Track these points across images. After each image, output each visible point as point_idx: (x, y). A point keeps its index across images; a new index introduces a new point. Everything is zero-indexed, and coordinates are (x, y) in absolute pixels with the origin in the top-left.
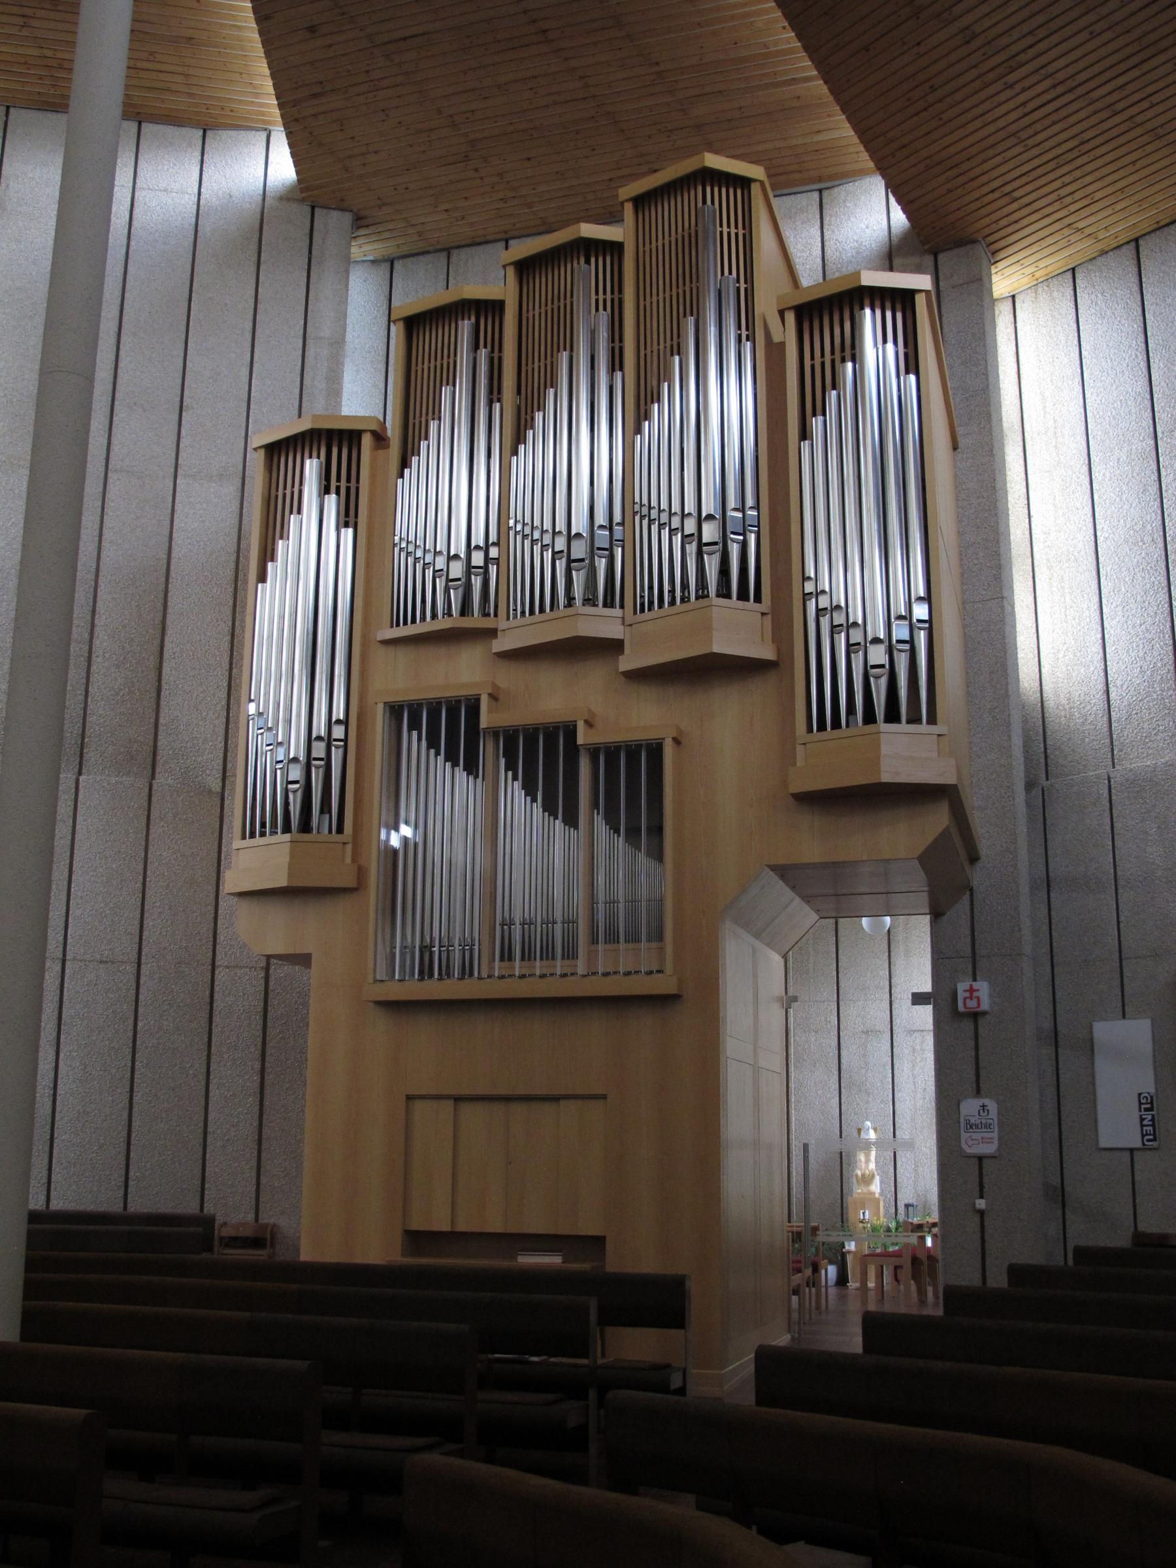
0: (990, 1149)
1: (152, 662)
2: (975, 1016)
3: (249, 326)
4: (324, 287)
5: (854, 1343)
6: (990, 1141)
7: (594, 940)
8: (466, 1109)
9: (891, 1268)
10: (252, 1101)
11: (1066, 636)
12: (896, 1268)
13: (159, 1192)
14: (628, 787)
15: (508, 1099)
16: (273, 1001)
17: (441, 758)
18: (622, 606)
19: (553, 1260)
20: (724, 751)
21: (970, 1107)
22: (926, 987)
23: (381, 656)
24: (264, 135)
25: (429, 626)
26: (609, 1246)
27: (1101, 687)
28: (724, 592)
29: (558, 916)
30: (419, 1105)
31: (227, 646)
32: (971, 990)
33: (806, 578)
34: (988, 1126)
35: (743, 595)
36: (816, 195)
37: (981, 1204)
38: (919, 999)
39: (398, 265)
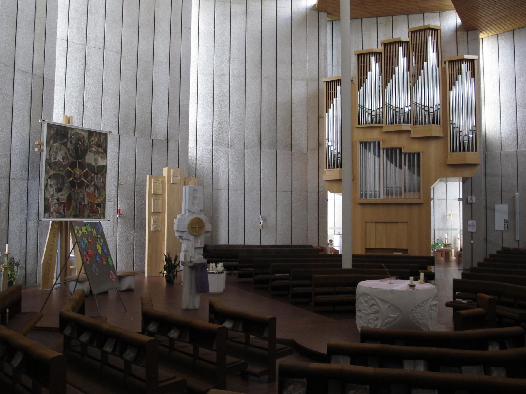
0: (474, 231)
1: (290, 124)
2: (472, 204)
4: (322, 32)
5: (411, 277)
6: (473, 229)
7: (405, 191)
9: (440, 255)
10: (316, 221)
12: (442, 254)
13: (298, 241)
14: (414, 161)
15: (386, 222)
16: (320, 200)
20: (432, 153)
21: (470, 222)
22: (461, 197)
23: (356, 131)
25: (367, 125)
26: (409, 251)
27: (500, 133)
28: (433, 123)
30: (368, 224)
31: (306, 120)
32: (471, 198)
33: (450, 121)
35: (437, 123)
36: (438, 13)
38: (459, 199)
39: (334, 22)
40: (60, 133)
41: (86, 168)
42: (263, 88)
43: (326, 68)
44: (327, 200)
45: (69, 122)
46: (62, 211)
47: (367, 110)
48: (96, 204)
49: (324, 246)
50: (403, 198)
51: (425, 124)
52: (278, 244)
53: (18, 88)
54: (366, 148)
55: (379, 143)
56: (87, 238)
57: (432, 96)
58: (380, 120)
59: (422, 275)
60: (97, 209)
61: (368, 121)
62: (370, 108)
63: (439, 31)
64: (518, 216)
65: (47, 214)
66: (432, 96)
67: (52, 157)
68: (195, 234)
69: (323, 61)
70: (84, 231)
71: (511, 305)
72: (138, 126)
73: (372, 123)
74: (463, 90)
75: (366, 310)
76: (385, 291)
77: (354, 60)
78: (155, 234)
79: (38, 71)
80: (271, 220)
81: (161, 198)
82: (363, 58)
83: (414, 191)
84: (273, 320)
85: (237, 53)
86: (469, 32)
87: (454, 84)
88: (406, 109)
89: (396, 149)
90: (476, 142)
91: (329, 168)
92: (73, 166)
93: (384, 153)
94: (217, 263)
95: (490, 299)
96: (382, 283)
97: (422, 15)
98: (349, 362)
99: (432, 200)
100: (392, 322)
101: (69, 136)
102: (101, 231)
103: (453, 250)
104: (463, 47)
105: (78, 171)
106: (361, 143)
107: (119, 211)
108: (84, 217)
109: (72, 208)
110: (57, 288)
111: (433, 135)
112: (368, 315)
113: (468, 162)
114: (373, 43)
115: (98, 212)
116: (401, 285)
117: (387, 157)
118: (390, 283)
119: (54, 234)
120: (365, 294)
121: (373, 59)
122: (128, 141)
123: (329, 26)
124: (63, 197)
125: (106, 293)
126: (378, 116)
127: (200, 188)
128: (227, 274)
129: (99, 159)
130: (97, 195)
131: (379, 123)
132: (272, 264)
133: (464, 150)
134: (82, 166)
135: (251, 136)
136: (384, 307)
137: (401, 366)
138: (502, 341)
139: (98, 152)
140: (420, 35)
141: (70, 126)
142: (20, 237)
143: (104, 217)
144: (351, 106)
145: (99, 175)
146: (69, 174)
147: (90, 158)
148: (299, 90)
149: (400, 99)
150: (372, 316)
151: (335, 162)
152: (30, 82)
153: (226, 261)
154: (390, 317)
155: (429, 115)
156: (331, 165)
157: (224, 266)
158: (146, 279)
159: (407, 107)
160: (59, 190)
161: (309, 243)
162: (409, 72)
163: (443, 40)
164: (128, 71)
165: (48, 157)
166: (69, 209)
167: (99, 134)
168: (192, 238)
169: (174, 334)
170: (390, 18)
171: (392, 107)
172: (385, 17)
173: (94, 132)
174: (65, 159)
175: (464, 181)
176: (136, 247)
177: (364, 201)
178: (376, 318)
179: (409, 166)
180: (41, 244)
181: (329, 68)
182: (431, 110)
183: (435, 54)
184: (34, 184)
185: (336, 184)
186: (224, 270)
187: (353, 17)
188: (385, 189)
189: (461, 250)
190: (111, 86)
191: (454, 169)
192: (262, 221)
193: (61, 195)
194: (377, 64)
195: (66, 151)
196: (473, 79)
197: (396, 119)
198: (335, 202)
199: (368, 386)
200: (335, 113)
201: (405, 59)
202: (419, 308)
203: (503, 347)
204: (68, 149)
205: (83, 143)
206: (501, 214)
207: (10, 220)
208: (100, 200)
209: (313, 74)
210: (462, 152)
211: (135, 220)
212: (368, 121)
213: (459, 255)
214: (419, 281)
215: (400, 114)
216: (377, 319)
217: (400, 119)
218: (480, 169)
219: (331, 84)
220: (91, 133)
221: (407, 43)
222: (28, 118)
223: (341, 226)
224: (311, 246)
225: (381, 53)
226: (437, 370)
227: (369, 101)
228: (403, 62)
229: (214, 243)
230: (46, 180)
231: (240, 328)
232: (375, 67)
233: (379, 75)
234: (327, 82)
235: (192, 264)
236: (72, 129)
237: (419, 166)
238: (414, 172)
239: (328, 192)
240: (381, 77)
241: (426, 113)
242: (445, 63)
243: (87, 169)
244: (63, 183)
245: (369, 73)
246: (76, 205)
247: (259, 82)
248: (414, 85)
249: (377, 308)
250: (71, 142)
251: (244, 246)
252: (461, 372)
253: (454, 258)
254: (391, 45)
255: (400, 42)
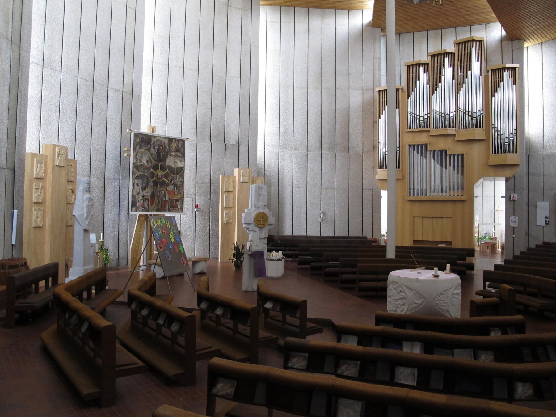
1: (347, 129)
2: (514, 201)
4: (377, 46)
7: (450, 189)
8: (425, 219)
10: (371, 215)
11: (536, 127)
13: (354, 232)
14: (459, 162)
19: (444, 246)
20: (475, 155)
21: (512, 218)
22: (504, 195)
25: (414, 130)
28: (476, 127)
30: (416, 218)
33: (492, 125)
35: (480, 127)
37: (514, 236)
38: (502, 197)
40: (144, 141)
41: (166, 170)
42: (324, 98)
45: (153, 132)
46: (146, 206)
48: (176, 200)
49: (377, 238)
52: (336, 235)
53: (111, 103)
54: (414, 150)
55: (426, 145)
56: (162, 230)
58: (427, 124)
59: (448, 266)
60: (176, 205)
63: (482, 42)
65: (134, 208)
66: (473, 101)
67: (138, 161)
68: (259, 226)
69: (377, 72)
70: (159, 223)
71: (535, 295)
72: (213, 132)
73: (420, 127)
74: (505, 95)
75: (394, 296)
76: (411, 280)
78: (227, 225)
79: (127, 89)
80: (330, 214)
81: (232, 195)
82: (412, 68)
84: (305, 303)
85: (300, 67)
87: (497, 91)
88: (452, 115)
90: (518, 143)
92: (155, 168)
94: (277, 251)
95: (510, 289)
97: (468, 28)
98: (356, 342)
100: (416, 308)
101: (152, 143)
102: (174, 223)
103: (500, 243)
105: (160, 173)
106: (410, 146)
107: (197, 206)
108: (165, 211)
109: (155, 203)
110: (143, 270)
111: (476, 138)
112: (397, 300)
113: (508, 163)
115: (177, 207)
116: (426, 275)
118: (418, 273)
119: (141, 225)
120: (394, 282)
122: (204, 146)
124: (147, 194)
125: (181, 275)
126: (426, 121)
127: (265, 187)
128: (286, 261)
129: (178, 162)
130: (176, 193)
131: (427, 127)
132: (325, 253)
134: (163, 168)
135: (313, 140)
136: (410, 294)
137: (400, 347)
138: (504, 327)
139: (177, 156)
141: (154, 134)
142: (113, 228)
143: (182, 211)
145: (178, 176)
146: (152, 175)
147: (170, 161)
148: (356, 99)
149: (445, 105)
150: (400, 302)
152: (121, 98)
153: (285, 250)
154: (415, 303)
155: (472, 119)
157: (283, 255)
158: (219, 264)
159: (453, 112)
160: (144, 188)
164: (204, 85)
165: (135, 161)
166: (152, 204)
167: (178, 140)
168: (257, 229)
169: (219, 311)
170: (440, 31)
172: (435, 31)
173: (173, 139)
174: (149, 162)
176: (211, 236)
177: (412, 198)
178: (402, 304)
179: (454, 167)
180: (130, 233)
183: (478, 64)
184: (124, 183)
186: (283, 258)
190: (190, 98)
191: (496, 169)
193: (146, 192)
194: (425, 74)
195: (150, 155)
199: (359, 362)
201: (451, 69)
202: (441, 296)
203: (504, 332)
204: (152, 154)
205: (164, 148)
206: (543, 209)
207: (105, 213)
208: (179, 197)
209: (368, 83)
210: (503, 154)
211: (209, 213)
216: (403, 305)
217: (445, 124)
218: (523, 169)
220: (171, 140)
221: (453, 54)
222: (120, 128)
224: (366, 238)
226: (431, 353)
227: (417, 107)
229: (280, 234)
230: (133, 180)
231: (278, 309)
232: (423, 77)
233: (427, 84)
234: (380, 91)
235: (250, 253)
236: (155, 137)
237: (462, 166)
240: (428, 86)
241: (470, 118)
242: (488, 71)
243: (167, 171)
244: (148, 183)
245: (418, 82)
246: (159, 201)
247: (320, 92)
249: (404, 294)
250: (154, 148)
251: (306, 237)
252: (453, 355)
255: (446, 54)
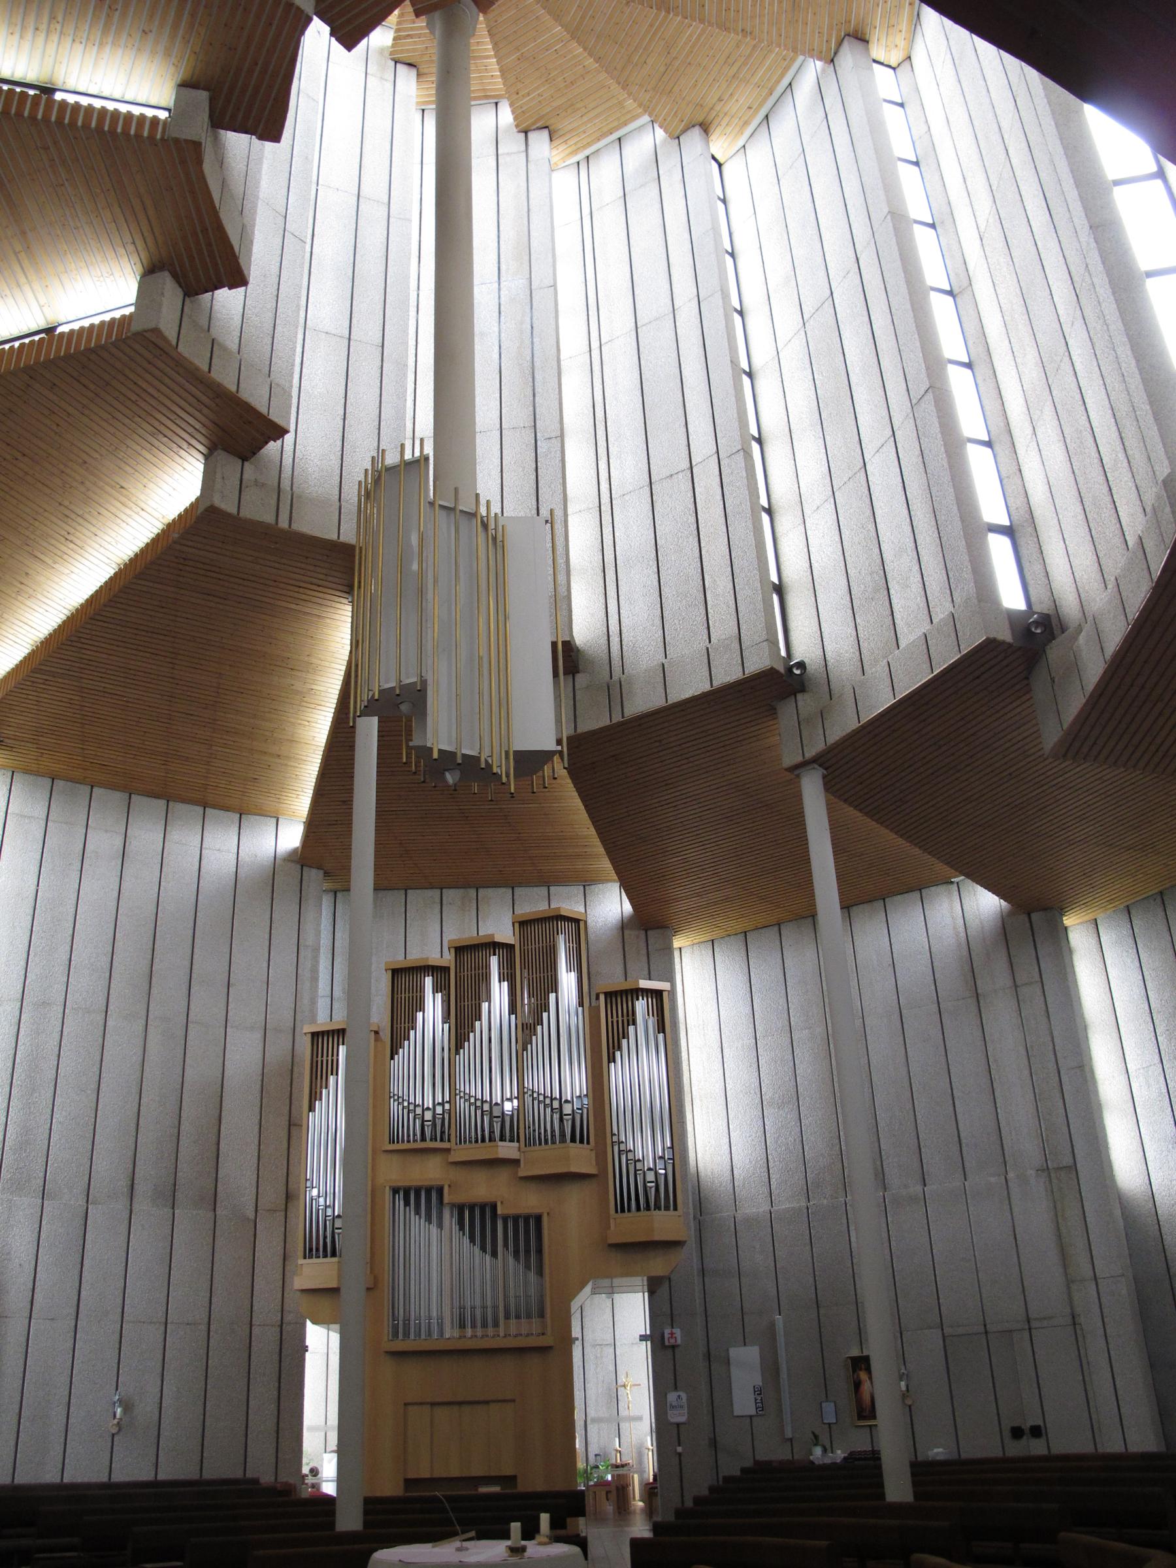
0: (683, 1419)
2: (673, 1347)
3: (267, 936)
4: (309, 915)
7: (507, 1317)
9: (604, 1493)
12: (607, 1493)
13: (220, 1468)
14: (527, 1237)
15: (460, 1403)
16: (285, 1346)
17: (423, 1220)
18: (518, 1141)
20: (571, 1218)
21: (672, 1397)
24: (274, 820)
25: (412, 1146)
27: (729, 1168)
28: (573, 1140)
29: (489, 1303)
30: (410, 1408)
32: (672, 1334)
33: (613, 1135)
34: (682, 1407)
35: (582, 1142)
37: (679, 1449)
39: (339, 895)
43: (313, 1002)
44: (306, 1349)
47: (411, 1108)
49: (291, 1481)
50: (502, 1334)
51: (554, 1142)
52: (161, 1477)
54: (407, 1203)
57: (574, 1082)
58: (443, 1133)
61: (415, 1135)
62: (419, 1101)
64: (784, 1375)
73: (423, 1139)
77: (381, 985)
80: (146, 1408)
83: (529, 1316)
86: (649, 932)
87: (620, 1048)
88: (508, 1106)
89: (483, 1207)
90: (674, 1185)
91: (311, 1257)
93: (452, 1216)
96: (437, 1550)
97: (544, 890)
99: (578, 1344)
104: (637, 965)
106: (395, 1191)
111: (574, 1169)
113: (657, 1238)
114: (430, 944)
117: (462, 1228)
118: (459, 1549)
121: (428, 982)
123: (327, 901)
126: (439, 1122)
131: (442, 1140)
133: (648, 1208)
135: (109, 1168)
140: (540, 930)
144: (370, 1096)
148: (244, 1055)
151: (329, 1240)
155: (561, 1120)
156: (317, 1250)
159: (510, 1100)
161: (250, 1475)
162: (513, 1017)
163: (592, 948)
171: (472, 1100)
175: (654, 1287)
177: (400, 1345)
181: (322, 1004)
182: (567, 1109)
183: (573, 976)
185: (326, 1302)
187: (380, 887)
188: (456, 1311)
189: (655, 1476)
191: (626, 1254)
192: (119, 1410)
196: (661, 1036)
197: (483, 1130)
198: (322, 1346)
200: (328, 1119)
210: (643, 1213)
212: (415, 1135)
213: (650, 1491)
214: (539, 1538)
215: (492, 1117)
217: (492, 1132)
219: (325, 1039)
221: (510, 947)
223: (336, 1423)
225: (449, 968)
227: (418, 1080)
228: (499, 992)
232: (433, 1008)
233: (444, 1022)
234: (315, 1035)
237: (540, 1251)
238: (527, 1267)
239: (308, 1323)
240: (446, 1026)
241: (556, 1116)
242: (598, 998)
245: (420, 1015)
247: (141, 1028)
248: (525, 1049)
251: (61, 1487)
253: (641, 1504)
254: (472, 952)
255: (494, 946)
